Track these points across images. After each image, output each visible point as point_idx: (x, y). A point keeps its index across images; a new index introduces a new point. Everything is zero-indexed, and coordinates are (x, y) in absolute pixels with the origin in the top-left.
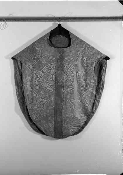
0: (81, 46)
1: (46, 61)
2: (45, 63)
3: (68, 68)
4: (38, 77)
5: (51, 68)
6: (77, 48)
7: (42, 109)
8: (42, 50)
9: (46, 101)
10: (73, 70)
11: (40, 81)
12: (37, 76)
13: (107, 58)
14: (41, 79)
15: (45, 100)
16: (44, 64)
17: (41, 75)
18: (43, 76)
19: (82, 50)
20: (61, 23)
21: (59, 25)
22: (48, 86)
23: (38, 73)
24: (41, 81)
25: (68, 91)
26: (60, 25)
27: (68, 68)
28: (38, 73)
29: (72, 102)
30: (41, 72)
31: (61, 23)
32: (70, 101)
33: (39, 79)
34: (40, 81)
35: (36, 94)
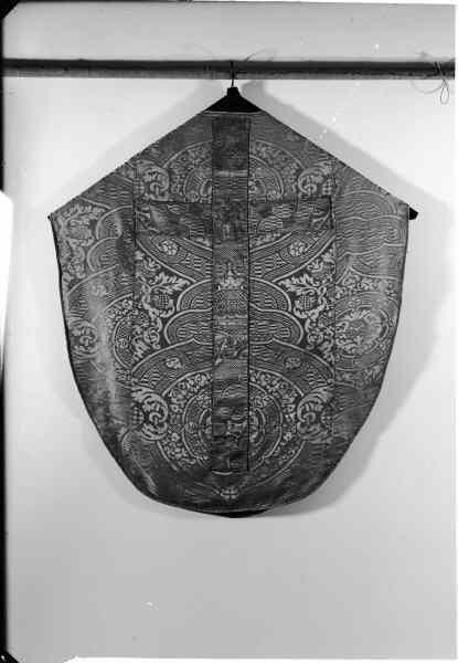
0: (312, 300)
1: (181, 361)
2: (179, 366)
3: (264, 160)
4: (151, 419)
5: (203, 160)
6: (298, 314)
7: (170, 313)
8: (164, 321)
9: (185, 286)
10: (283, 164)
11: (157, 438)
12: (147, 414)
13: (413, 214)
14: (160, 430)
15: (181, 282)
16: (172, 368)
17: (161, 412)
18: (167, 421)
19: (314, 318)
20: (239, 84)
21: (229, 90)
22: (187, 460)
23: (150, 403)
24: (160, 438)
25: (266, 243)
26: (233, 91)
27: (265, 388)
28: (150, 403)
29: (283, 287)
30: (162, 401)
31: (239, 84)
32: (276, 283)
33: (153, 429)
34: (157, 438)
35: (143, 252)
